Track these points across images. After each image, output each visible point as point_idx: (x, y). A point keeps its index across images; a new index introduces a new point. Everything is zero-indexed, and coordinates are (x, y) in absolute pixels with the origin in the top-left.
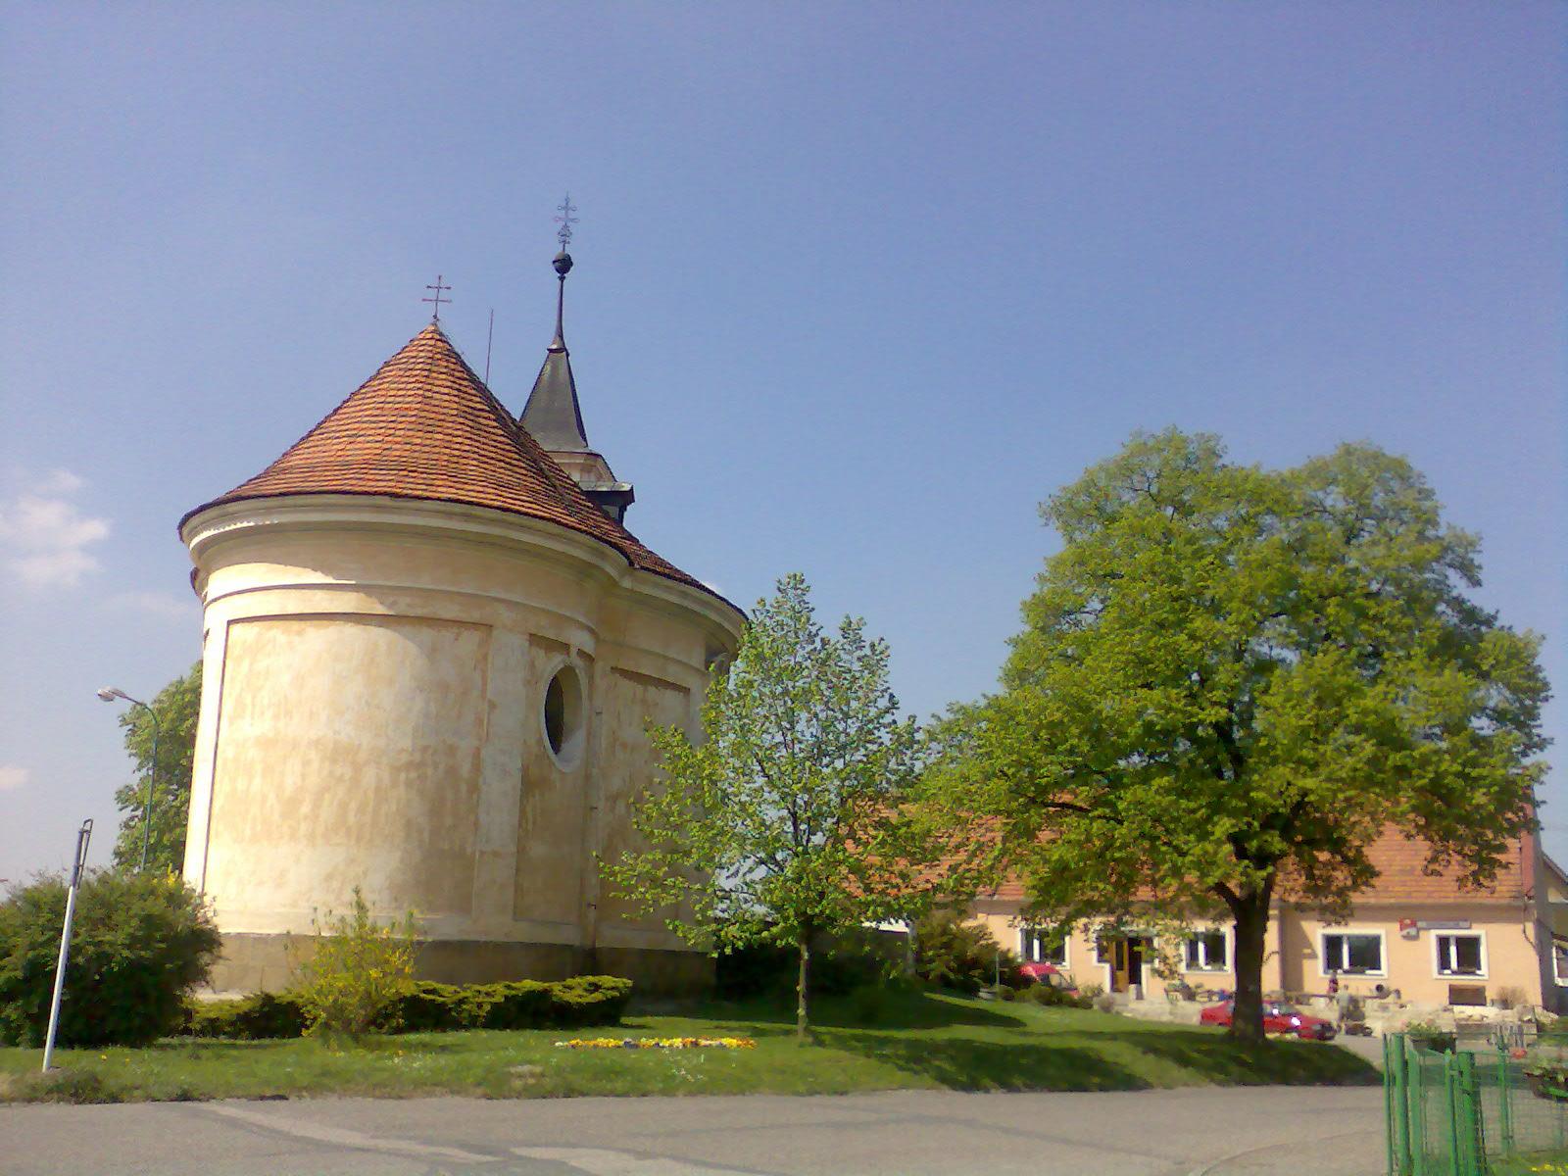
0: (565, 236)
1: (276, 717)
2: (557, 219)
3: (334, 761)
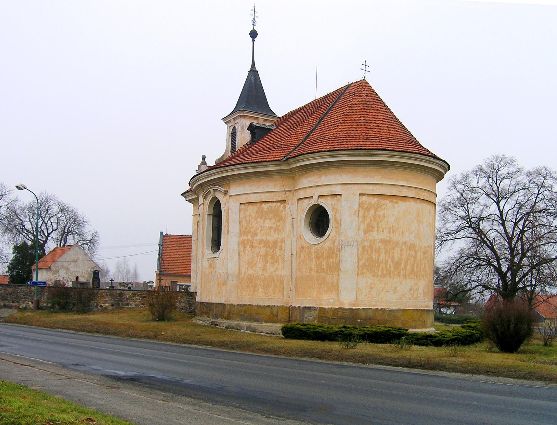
1: (389, 233)
3: (410, 250)
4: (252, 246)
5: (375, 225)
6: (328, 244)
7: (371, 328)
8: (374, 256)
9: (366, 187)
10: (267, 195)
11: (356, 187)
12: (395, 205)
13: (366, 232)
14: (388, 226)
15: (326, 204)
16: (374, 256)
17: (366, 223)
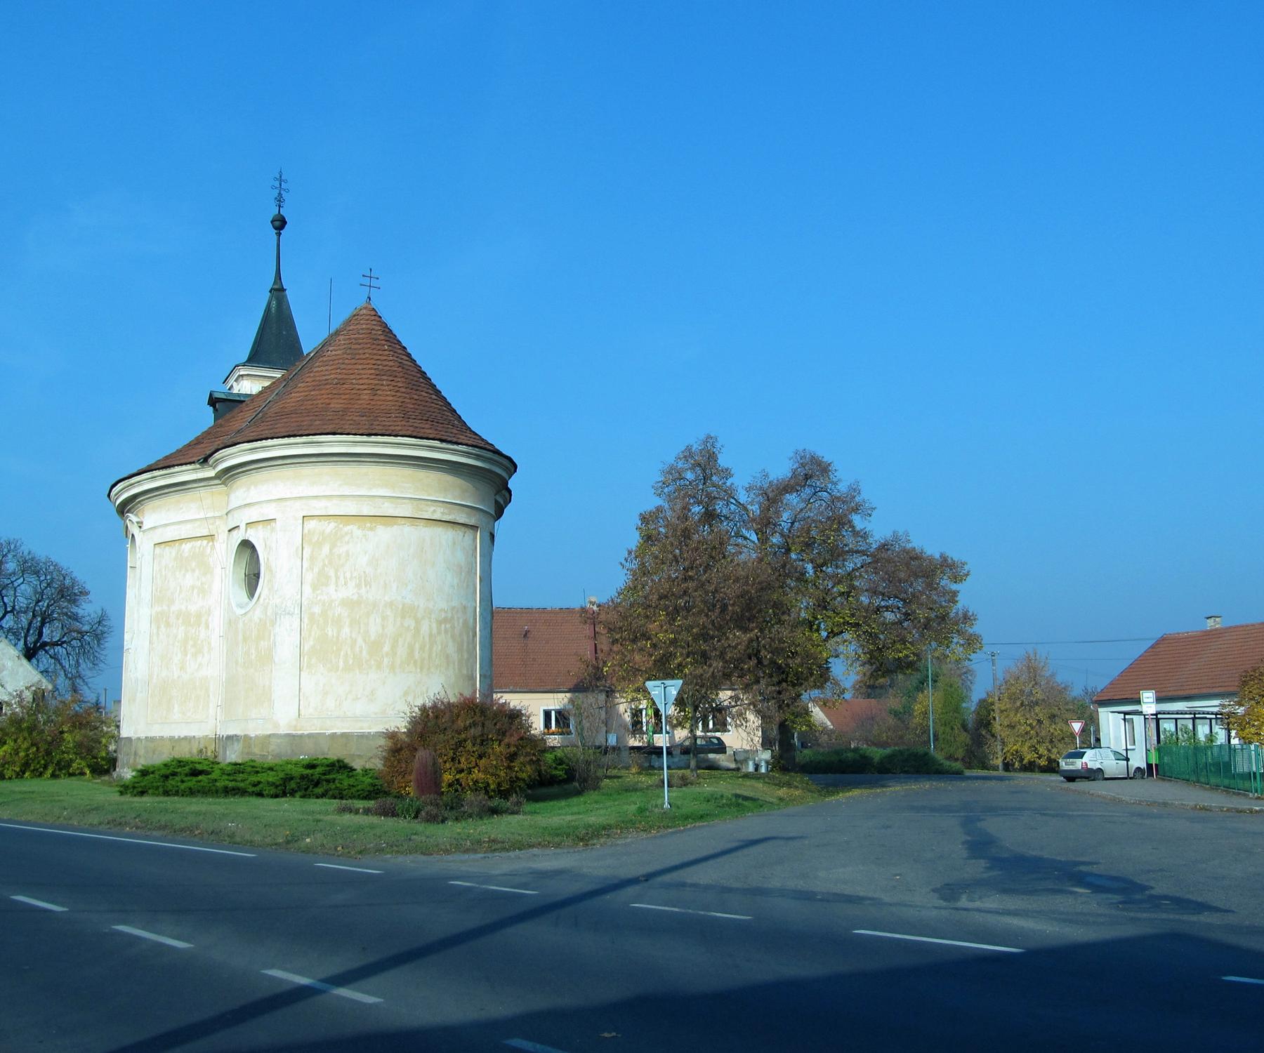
0: (280, 201)
1: (358, 586)
2: (273, 187)
3: (403, 617)
4: (168, 625)
5: (332, 573)
6: (258, 615)
7: (555, 789)
8: (331, 631)
9: (314, 503)
10: (189, 526)
11: (298, 504)
12: (370, 533)
13: (315, 588)
14: (355, 574)
15: (255, 537)
16: (330, 633)
17: (316, 570)
